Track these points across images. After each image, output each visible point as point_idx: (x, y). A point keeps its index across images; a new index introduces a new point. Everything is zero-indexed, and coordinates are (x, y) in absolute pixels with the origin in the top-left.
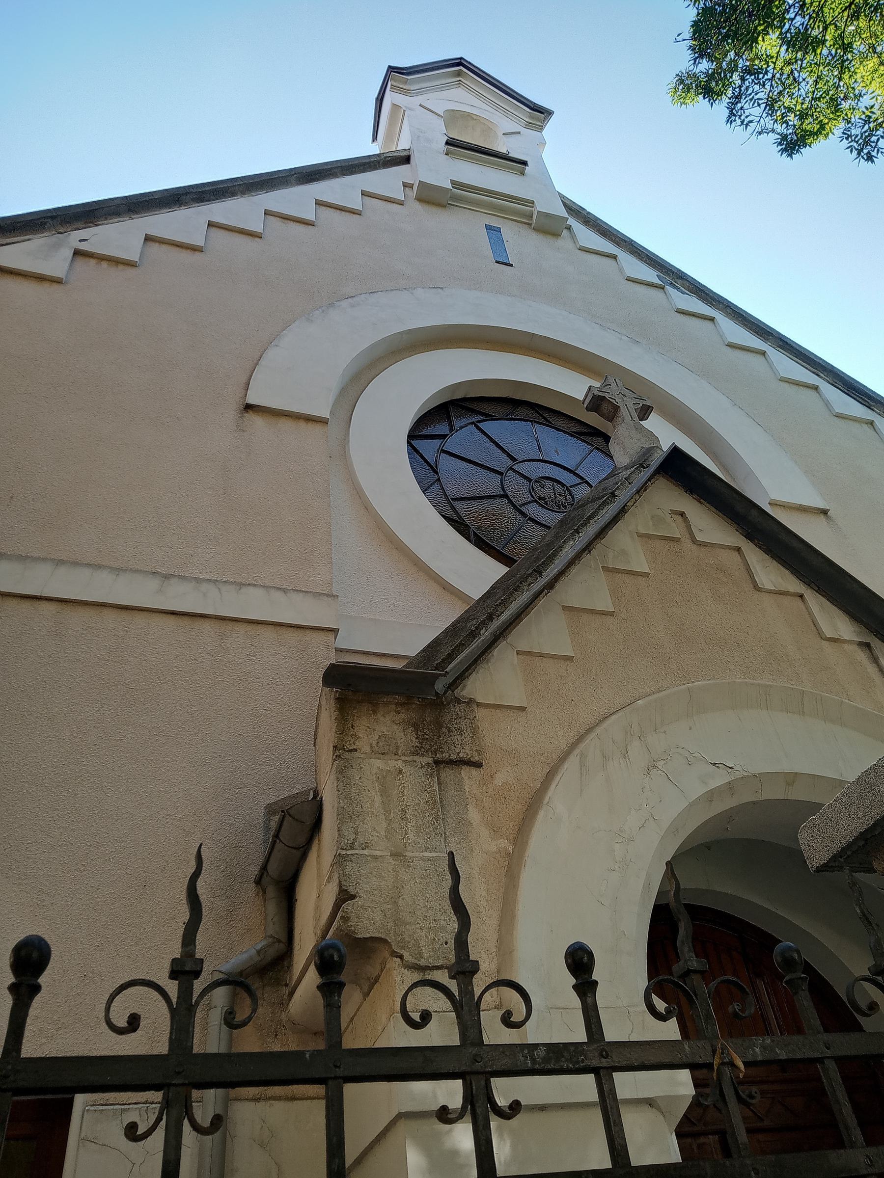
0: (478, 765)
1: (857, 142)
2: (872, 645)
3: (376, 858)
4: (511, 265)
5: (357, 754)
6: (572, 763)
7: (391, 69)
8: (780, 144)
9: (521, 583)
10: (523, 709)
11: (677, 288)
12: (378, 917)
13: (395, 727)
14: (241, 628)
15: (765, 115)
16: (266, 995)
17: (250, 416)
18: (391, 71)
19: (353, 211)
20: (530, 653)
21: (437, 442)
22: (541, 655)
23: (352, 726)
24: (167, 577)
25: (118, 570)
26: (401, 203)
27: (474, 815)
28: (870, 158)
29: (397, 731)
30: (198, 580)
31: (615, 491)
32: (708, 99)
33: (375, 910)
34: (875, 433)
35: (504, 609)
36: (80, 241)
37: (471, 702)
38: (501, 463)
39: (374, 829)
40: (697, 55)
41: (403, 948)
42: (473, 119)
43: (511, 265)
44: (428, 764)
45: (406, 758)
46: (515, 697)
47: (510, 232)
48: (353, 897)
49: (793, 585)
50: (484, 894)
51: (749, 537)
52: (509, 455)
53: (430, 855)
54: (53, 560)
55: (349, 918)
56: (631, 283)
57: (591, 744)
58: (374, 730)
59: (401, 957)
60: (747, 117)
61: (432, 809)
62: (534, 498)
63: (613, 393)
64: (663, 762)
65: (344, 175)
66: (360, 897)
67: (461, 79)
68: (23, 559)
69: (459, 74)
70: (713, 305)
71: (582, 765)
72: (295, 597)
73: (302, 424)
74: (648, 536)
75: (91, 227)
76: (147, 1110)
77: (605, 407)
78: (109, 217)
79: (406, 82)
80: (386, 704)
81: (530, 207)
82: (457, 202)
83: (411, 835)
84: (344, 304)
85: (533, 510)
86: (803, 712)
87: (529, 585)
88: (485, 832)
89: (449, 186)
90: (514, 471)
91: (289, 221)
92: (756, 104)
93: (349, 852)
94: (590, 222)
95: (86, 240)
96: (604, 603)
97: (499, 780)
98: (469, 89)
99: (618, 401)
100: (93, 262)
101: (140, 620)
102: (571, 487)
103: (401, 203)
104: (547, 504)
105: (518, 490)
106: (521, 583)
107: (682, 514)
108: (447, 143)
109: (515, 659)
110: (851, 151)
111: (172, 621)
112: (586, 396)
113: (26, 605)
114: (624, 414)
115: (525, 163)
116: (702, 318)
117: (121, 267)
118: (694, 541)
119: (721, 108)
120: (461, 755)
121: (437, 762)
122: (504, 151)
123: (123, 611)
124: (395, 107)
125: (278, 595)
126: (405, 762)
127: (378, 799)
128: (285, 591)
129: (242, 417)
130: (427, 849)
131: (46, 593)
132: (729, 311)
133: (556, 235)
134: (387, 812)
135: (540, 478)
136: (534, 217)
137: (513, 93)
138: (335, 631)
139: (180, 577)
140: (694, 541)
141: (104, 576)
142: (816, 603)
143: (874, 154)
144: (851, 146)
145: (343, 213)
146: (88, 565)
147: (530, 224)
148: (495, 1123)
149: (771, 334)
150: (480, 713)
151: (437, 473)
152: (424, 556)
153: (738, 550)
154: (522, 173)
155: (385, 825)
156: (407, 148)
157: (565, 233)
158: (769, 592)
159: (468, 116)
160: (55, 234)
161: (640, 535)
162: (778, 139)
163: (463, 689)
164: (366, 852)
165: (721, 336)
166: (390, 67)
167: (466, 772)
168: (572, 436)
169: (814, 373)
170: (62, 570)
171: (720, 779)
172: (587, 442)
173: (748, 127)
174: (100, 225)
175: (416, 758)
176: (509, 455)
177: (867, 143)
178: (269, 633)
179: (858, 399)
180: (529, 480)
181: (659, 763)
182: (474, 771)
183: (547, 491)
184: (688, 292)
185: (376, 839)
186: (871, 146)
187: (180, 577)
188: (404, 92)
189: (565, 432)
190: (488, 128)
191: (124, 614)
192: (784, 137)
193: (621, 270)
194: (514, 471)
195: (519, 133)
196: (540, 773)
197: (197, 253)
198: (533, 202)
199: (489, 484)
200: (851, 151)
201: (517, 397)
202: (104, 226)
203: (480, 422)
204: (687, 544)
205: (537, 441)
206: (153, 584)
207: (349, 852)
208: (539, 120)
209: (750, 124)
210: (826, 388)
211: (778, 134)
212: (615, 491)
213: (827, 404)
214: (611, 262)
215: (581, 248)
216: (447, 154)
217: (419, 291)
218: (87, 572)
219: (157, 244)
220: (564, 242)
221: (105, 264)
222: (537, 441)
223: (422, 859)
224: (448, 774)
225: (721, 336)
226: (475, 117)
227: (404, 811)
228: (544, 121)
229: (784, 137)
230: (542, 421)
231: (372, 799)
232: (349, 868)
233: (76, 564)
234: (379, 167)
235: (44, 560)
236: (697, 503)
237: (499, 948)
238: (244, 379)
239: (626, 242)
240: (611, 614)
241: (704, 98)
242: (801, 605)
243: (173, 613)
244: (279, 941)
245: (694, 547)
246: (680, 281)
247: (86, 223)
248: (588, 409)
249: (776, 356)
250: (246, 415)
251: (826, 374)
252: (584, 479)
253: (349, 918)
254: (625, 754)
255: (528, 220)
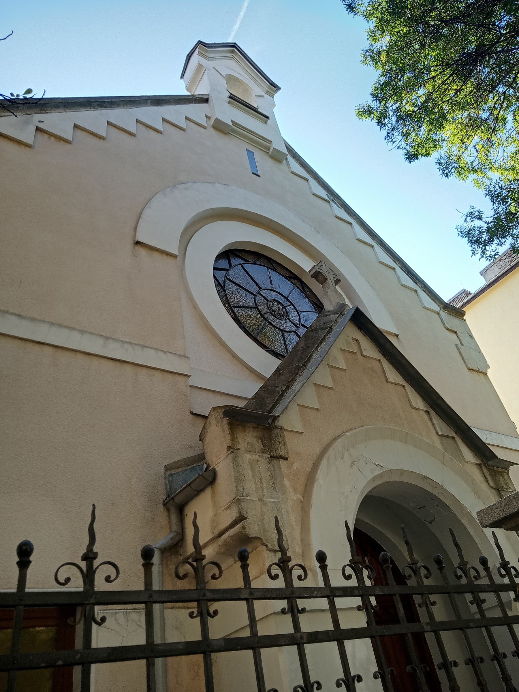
0: (286, 459)
1: (442, 166)
2: (430, 412)
3: (253, 501)
4: (260, 176)
5: (240, 451)
6: (324, 462)
7: (200, 42)
8: (406, 155)
9: (298, 371)
10: (302, 433)
11: (336, 204)
12: (256, 528)
13: (254, 439)
14: (145, 371)
15: (403, 140)
16: (172, 559)
17: (138, 248)
18: (200, 44)
19: (183, 129)
20: (302, 406)
21: (224, 272)
22: (306, 407)
23: (236, 437)
24: (107, 338)
25: (83, 332)
26: (205, 128)
27: (287, 482)
28: (447, 176)
29: (255, 441)
30: (123, 342)
31: (331, 326)
32: (380, 126)
33: (255, 525)
34: (417, 296)
35: (293, 383)
36: (39, 121)
37: (282, 428)
38: (254, 289)
39: (251, 487)
40: (375, 99)
41: (268, 542)
42: (240, 82)
43: (260, 176)
44: (268, 458)
45: (260, 454)
46: (299, 428)
47: (258, 155)
48: (246, 518)
49: (401, 381)
50: (294, 519)
51: (384, 355)
52: (257, 285)
53: (273, 500)
54: (48, 322)
55: (245, 528)
56: (315, 196)
57: (331, 453)
58: (245, 439)
59: (267, 546)
60: (394, 139)
61: (272, 479)
62: (270, 311)
63: (324, 270)
64: (357, 462)
65: (176, 104)
66: (249, 518)
67: (233, 55)
68: (33, 320)
69: (233, 52)
70: (351, 216)
71: (328, 462)
72: (169, 355)
73: (165, 256)
74: (344, 350)
75: (44, 113)
76: (126, 613)
77: (320, 278)
78: (53, 109)
79: (207, 51)
80: (249, 427)
81: (269, 144)
82: (233, 133)
83: (265, 491)
84: (181, 187)
85: (269, 317)
86: (407, 442)
87: (302, 372)
88: (291, 490)
89: (231, 124)
90: (260, 294)
91: (149, 129)
92: (400, 134)
93: (242, 498)
94: (296, 157)
95: (42, 122)
96: (330, 384)
97: (295, 466)
98: (237, 62)
99: (327, 275)
100: (46, 136)
101: (96, 361)
102: (286, 306)
103: (205, 128)
104: (275, 315)
105: (262, 305)
106: (298, 371)
107: (357, 340)
108: (230, 97)
109: (297, 408)
110: (440, 170)
111: (111, 363)
112: (312, 269)
113: (37, 347)
114: (330, 283)
115: (268, 118)
116: (346, 222)
117: (62, 142)
118: (362, 355)
119: (384, 132)
120: (281, 454)
121: (271, 457)
122: (256, 107)
123: (87, 355)
124: (200, 66)
125: (161, 354)
126: (259, 456)
127: (250, 473)
128: (165, 352)
129: (134, 248)
130: (272, 498)
131: (47, 341)
132: (358, 220)
133: (280, 161)
134: (255, 479)
135: (273, 300)
136: (270, 150)
137: (261, 72)
138: (189, 376)
139: (114, 339)
140: (362, 355)
141: (76, 335)
142: (410, 390)
143: (449, 174)
144: (440, 168)
145: (176, 128)
146: (67, 327)
147: (268, 153)
148: (94, 626)
149: (377, 237)
150: (286, 433)
151: (225, 291)
152: (224, 338)
153: (379, 361)
154: (266, 123)
155: (254, 486)
156: (207, 94)
157: (284, 161)
158: (392, 383)
159: (238, 80)
160: (25, 114)
161: (341, 350)
162: (405, 152)
163: (278, 422)
164: (248, 498)
165: (355, 234)
166: (199, 41)
167: (282, 462)
168: (286, 278)
169: (394, 261)
170: (54, 329)
171: (378, 472)
172: (292, 282)
173: (394, 143)
174: (49, 113)
175: (263, 454)
176: (257, 285)
177: (447, 168)
178: (158, 374)
179: (411, 277)
180: (267, 300)
181: (355, 463)
182: (285, 462)
183: (275, 307)
184: (340, 207)
185: (251, 491)
186: (448, 170)
187: (114, 339)
188: (206, 57)
189: (283, 276)
190: (246, 90)
191: (87, 357)
192: (408, 152)
193: (310, 188)
194: (260, 294)
195: (263, 96)
196: (310, 464)
197: (102, 140)
198: (271, 142)
199: (249, 300)
200: (440, 170)
201: (261, 252)
202: (52, 114)
203: (243, 264)
204: (359, 356)
205: (270, 278)
206: (100, 341)
207: (242, 498)
208: (273, 91)
209: (395, 142)
210: (398, 269)
211: (406, 150)
212: (331, 326)
213: (399, 278)
214: (305, 182)
215: (292, 172)
216: (229, 103)
217: (217, 185)
218: (66, 331)
219: (80, 131)
220: (284, 166)
221: (53, 139)
222: (270, 278)
223: (271, 502)
224: (275, 462)
225: (354, 234)
226: (241, 81)
227: (261, 480)
228: (276, 92)
229: (408, 152)
230: (272, 268)
231: (248, 473)
232: (244, 505)
233: (60, 326)
234: (192, 101)
235: (44, 321)
236: (363, 335)
237: (302, 543)
238: (133, 225)
239: (313, 173)
240: (332, 389)
241: (378, 125)
242: (403, 390)
243: (112, 359)
244: (180, 534)
245: (362, 358)
246: (336, 200)
247: (41, 110)
248: (312, 276)
249: (378, 249)
250: (136, 247)
251: (399, 262)
252: (292, 303)
253: (245, 528)
254: (343, 457)
255: (267, 150)
